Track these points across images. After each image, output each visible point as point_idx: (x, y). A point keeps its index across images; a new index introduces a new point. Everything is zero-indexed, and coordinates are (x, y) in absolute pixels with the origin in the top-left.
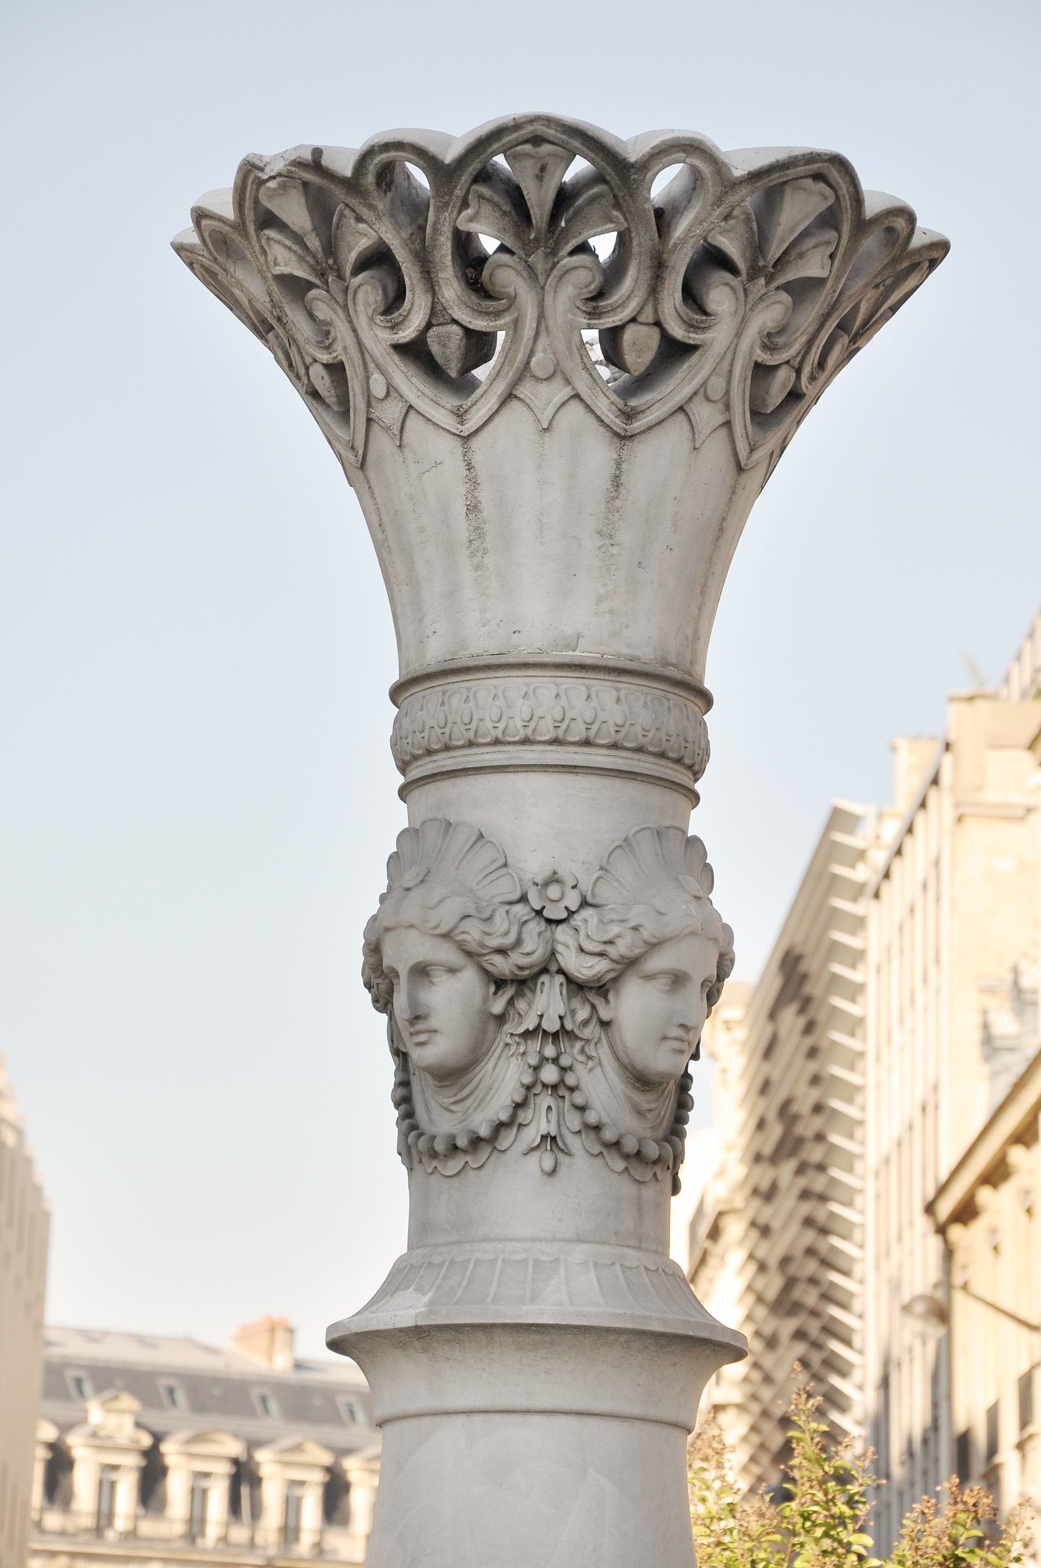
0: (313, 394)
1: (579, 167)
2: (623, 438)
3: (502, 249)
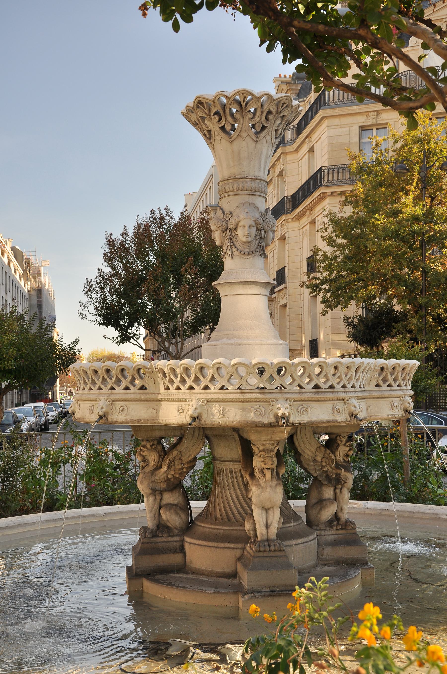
0: (204, 135)
1: (249, 97)
2: (256, 142)
3: (237, 111)
